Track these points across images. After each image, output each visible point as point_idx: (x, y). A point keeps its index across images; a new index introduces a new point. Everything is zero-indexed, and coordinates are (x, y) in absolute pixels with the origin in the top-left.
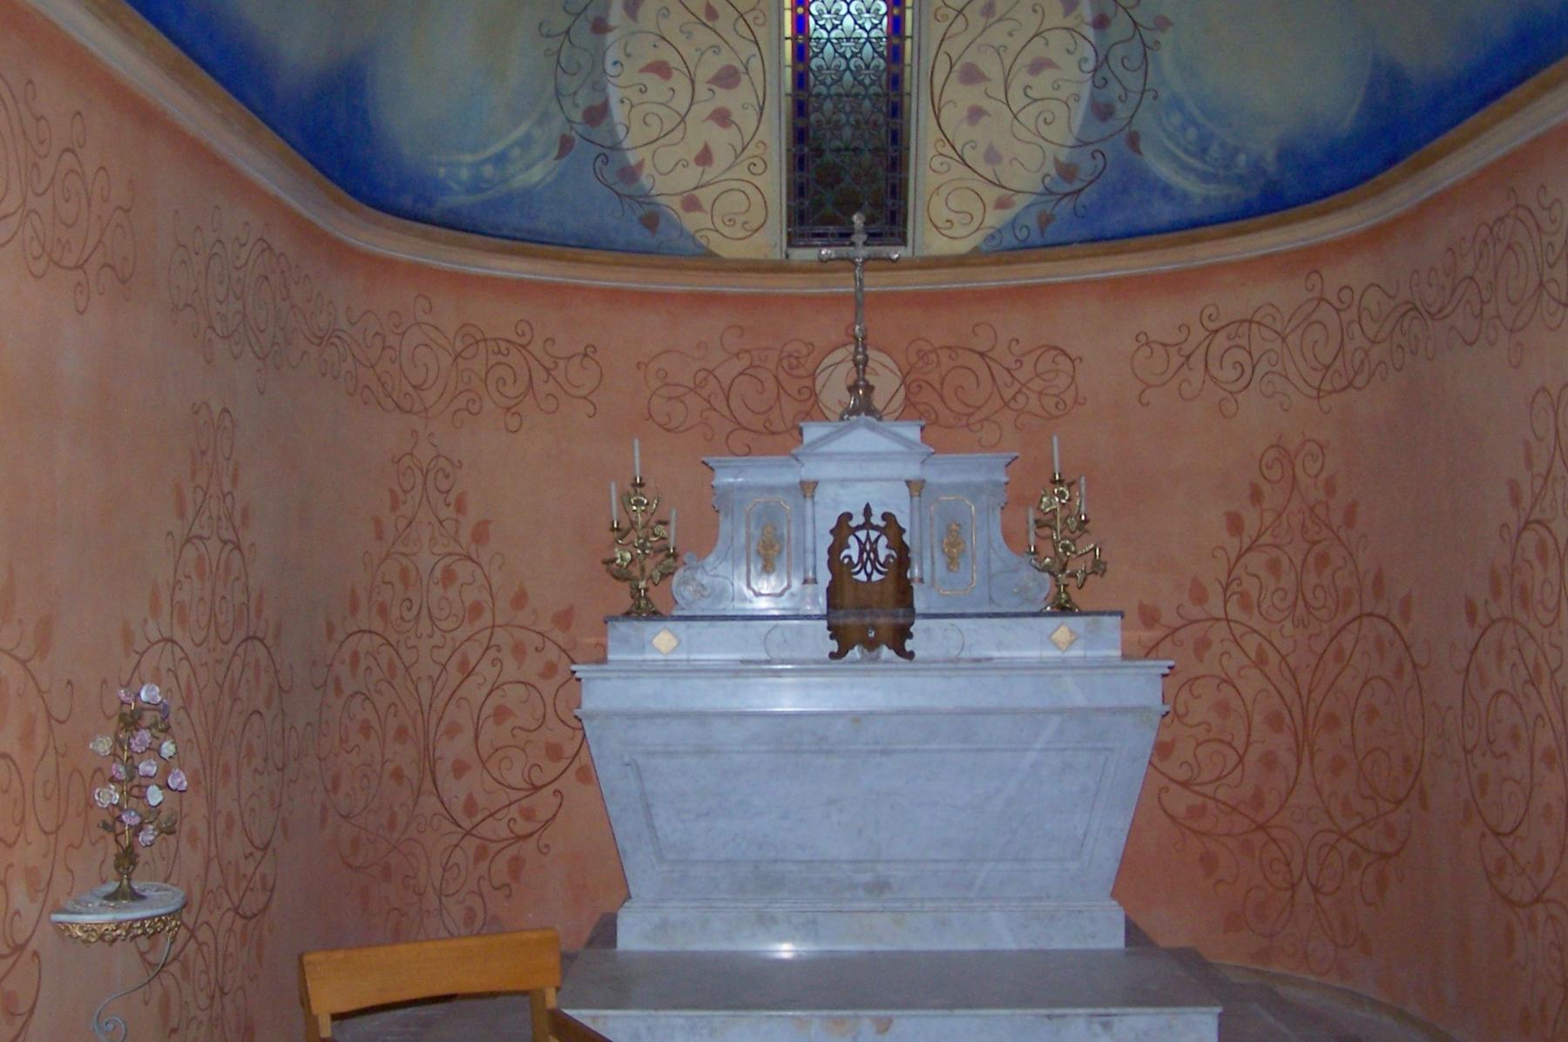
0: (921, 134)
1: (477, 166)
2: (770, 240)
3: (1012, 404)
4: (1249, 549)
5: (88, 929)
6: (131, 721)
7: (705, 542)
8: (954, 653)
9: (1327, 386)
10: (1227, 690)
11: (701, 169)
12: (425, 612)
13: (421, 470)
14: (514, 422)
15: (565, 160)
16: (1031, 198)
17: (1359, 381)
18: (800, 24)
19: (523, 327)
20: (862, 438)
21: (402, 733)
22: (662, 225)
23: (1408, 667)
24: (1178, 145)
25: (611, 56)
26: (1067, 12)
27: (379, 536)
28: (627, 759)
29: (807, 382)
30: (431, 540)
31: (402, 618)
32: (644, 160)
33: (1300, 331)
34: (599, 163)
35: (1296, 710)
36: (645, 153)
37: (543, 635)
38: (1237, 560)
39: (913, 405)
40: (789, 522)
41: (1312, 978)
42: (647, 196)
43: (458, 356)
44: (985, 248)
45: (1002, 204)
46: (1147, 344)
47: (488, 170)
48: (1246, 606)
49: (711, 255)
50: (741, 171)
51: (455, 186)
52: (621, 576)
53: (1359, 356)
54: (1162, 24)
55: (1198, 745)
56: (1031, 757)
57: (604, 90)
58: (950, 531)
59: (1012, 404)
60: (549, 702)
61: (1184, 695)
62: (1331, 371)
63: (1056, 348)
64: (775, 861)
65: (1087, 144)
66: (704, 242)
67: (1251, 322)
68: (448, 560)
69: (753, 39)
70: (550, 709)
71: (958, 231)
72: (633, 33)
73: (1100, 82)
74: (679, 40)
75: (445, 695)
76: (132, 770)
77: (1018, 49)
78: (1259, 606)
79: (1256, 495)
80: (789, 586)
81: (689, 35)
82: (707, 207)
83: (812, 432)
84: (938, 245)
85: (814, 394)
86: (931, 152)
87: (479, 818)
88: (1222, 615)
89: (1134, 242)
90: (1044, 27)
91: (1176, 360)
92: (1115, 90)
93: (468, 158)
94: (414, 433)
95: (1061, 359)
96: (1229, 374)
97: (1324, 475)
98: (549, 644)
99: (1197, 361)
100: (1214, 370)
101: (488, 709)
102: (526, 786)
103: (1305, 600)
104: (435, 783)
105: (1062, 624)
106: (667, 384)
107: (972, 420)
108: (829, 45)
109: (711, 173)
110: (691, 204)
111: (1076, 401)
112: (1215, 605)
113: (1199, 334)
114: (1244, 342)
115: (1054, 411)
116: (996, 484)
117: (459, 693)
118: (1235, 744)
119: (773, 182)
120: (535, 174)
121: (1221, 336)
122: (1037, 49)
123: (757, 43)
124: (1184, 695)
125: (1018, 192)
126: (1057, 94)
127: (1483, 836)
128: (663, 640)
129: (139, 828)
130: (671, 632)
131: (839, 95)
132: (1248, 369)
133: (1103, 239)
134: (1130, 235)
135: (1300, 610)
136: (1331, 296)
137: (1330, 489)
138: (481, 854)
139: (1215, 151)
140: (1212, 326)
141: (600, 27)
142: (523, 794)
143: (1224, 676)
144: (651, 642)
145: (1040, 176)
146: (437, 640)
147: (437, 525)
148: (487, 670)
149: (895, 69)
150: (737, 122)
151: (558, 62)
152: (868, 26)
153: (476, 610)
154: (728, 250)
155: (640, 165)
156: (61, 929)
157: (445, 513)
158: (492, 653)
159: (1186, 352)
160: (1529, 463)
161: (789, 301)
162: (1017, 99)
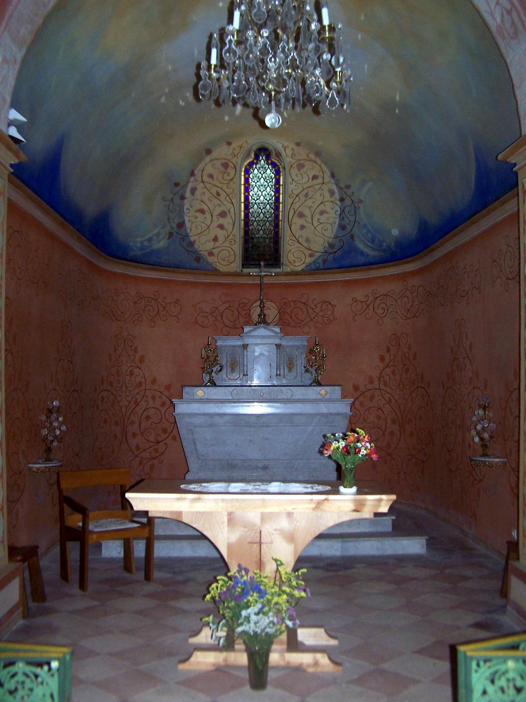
0: (285, 233)
1: (142, 243)
2: (236, 266)
3: (314, 320)
4: (386, 367)
5: (38, 469)
6: (50, 411)
8: (289, 397)
9: (408, 316)
10: (380, 411)
11: (214, 243)
12: (124, 384)
13: (123, 339)
14: (153, 324)
15: (170, 240)
16: (321, 254)
17: (417, 315)
18: (247, 198)
19: (156, 293)
20: (262, 331)
21: (116, 423)
22: (201, 260)
23: (429, 403)
24: (366, 239)
25: (185, 207)
26: (331, 197)
27: (110, 360)
28: (189, 428)
29: (248, 312)
30: (126, 361)
31: (117, 386)
32: (196, 240)
33: (401, 298)
34: (181, 241)
35: (400, 418)
36: (196, 238)
37: (161, 393)
38: (383, 370)
39: (282, 319)
40: (239, 357)
41: (403, 501)
42: (197, 251)
43: (135, 303)
44: (305, 269)
45: (311, 255)
46: (356, 301)
47: (146, 243)
48: (385, 385)
49: (216, 270)
50: (227, 244)
51: (135, 248)
53: (417, 307)
54: (360, 201)
55: (371, 429)
56: (311, 428)
57: (183, 217)
58: (289, 360)
59: (314, 320)
60: (163, 414)
61: (367, 413)
62: (410, 311)
63: (328, 302)
64: (234, 460)
65: (338, 237)
66: (215, 266)
67: (387, 295)
68: (131, 368)
69: (231, 202)
70: (163, 416)
71: (296, 264)
72: (193, 200)
73: (342, 218)
74: (208, 202)
75: (130, 411)
76: (51, 424)
77: (316, 207)
78: (389, 385)
79: (388, 350)
80: (239, 377)
81: (211, 201)
82: (216, 255)
83: (247, 329)
85: (250, 316)
86: (288, 239)
87: (140, 451)
88: (378, 388)
89: (352, 269)
90: (324, 200)
91: (365, 307)
92: (346, 221)
93: (139, 239)
94: (121, 327)
95: (329, 306)
96: (380, 311)
97: (408, 343)
98: (163, 396)
99: (371, 306)
100: (376, 310)
101: (144, 416)
102: (155, 441)
103: (403, 384)
104: (126, 439)
105: (323, 389)
106: (203, 312)
107: (301, 324)
108: (256, 205)
109: (217, 244)
111: (334, 320)
112: (376, 384)
113: (371, 299)
114: (385, 301)
115: (327, 323)
116: (304, 346)
117: (134, 411)
118: (382, 428)
119: (238, 248)
120: (161, 244)
121: (378, 299)
122: (322, 207)
123: (233, 204)
124: (367, 413)
125: (316, 252)
126: (328, 222)
127: (446, 453)
129: (52, 441)
130: (202, 390)
131: (259, 221)
132: (386, 310)
133: (343, 268)
134: (351, 267)
135: (401, 386)
136: (410, 289)
137: (409, 348)
138: (141, 463)
139: (376, 242)
140: (375, 296)
141: (183, 198)
142: (154, 444)
143: (378, 407)
144: (196, 393)
145: (323, 247)
146: (128, 394)
147: (128, 356)
148: (143, 404)
149: (277, 213)
150: (226, 228)
151: (169, 208)
152: (268, 199)
153: (140, 384)
154: (223, 269)
155: (195, 241)
156: (30, 469)
157: (131, 353)
158: (145, 398)
159: (367, 304)
160: (455, 342)
161: (241, 285)
162: (316, 223)
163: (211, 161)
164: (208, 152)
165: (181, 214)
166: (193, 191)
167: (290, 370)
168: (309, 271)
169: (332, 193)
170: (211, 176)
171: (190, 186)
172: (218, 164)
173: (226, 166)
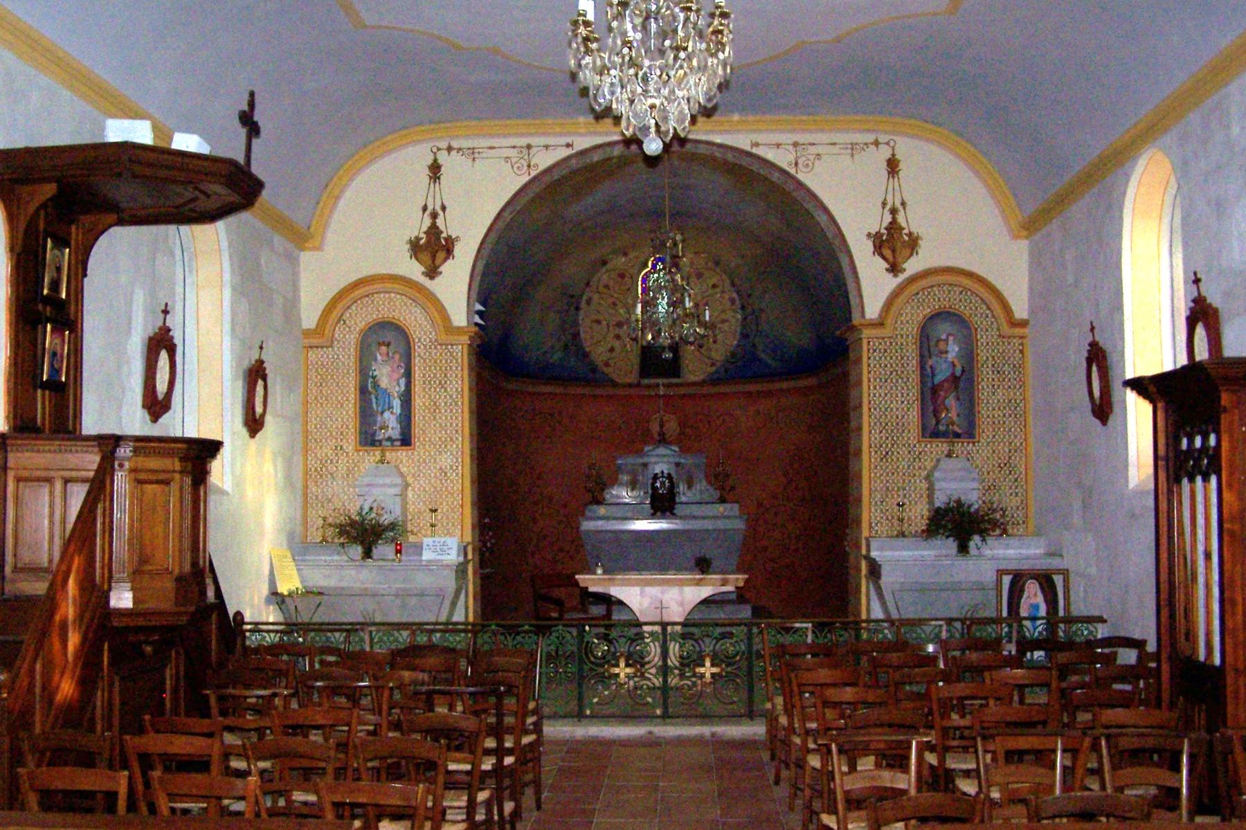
2: (633, 378)
7: (614, 481)
20: (662, 450)
45: (713, 365)
47: (541, 358)
52: (589, 491)
71: (697, 374)
84: (692, 378)
110: (607, 364)
120: (556, 357)
128: (602, 510)
141: (578, 309)
163: (607, 271)
164: (605, 263)
165: (576, 323)
166: (589, 302)
167: (690, 487)
168: (713, 381)
169: (733, 301)
170: (606, 286)
171: (585, 297)
172: (614, 275)
173: (622, 276)
